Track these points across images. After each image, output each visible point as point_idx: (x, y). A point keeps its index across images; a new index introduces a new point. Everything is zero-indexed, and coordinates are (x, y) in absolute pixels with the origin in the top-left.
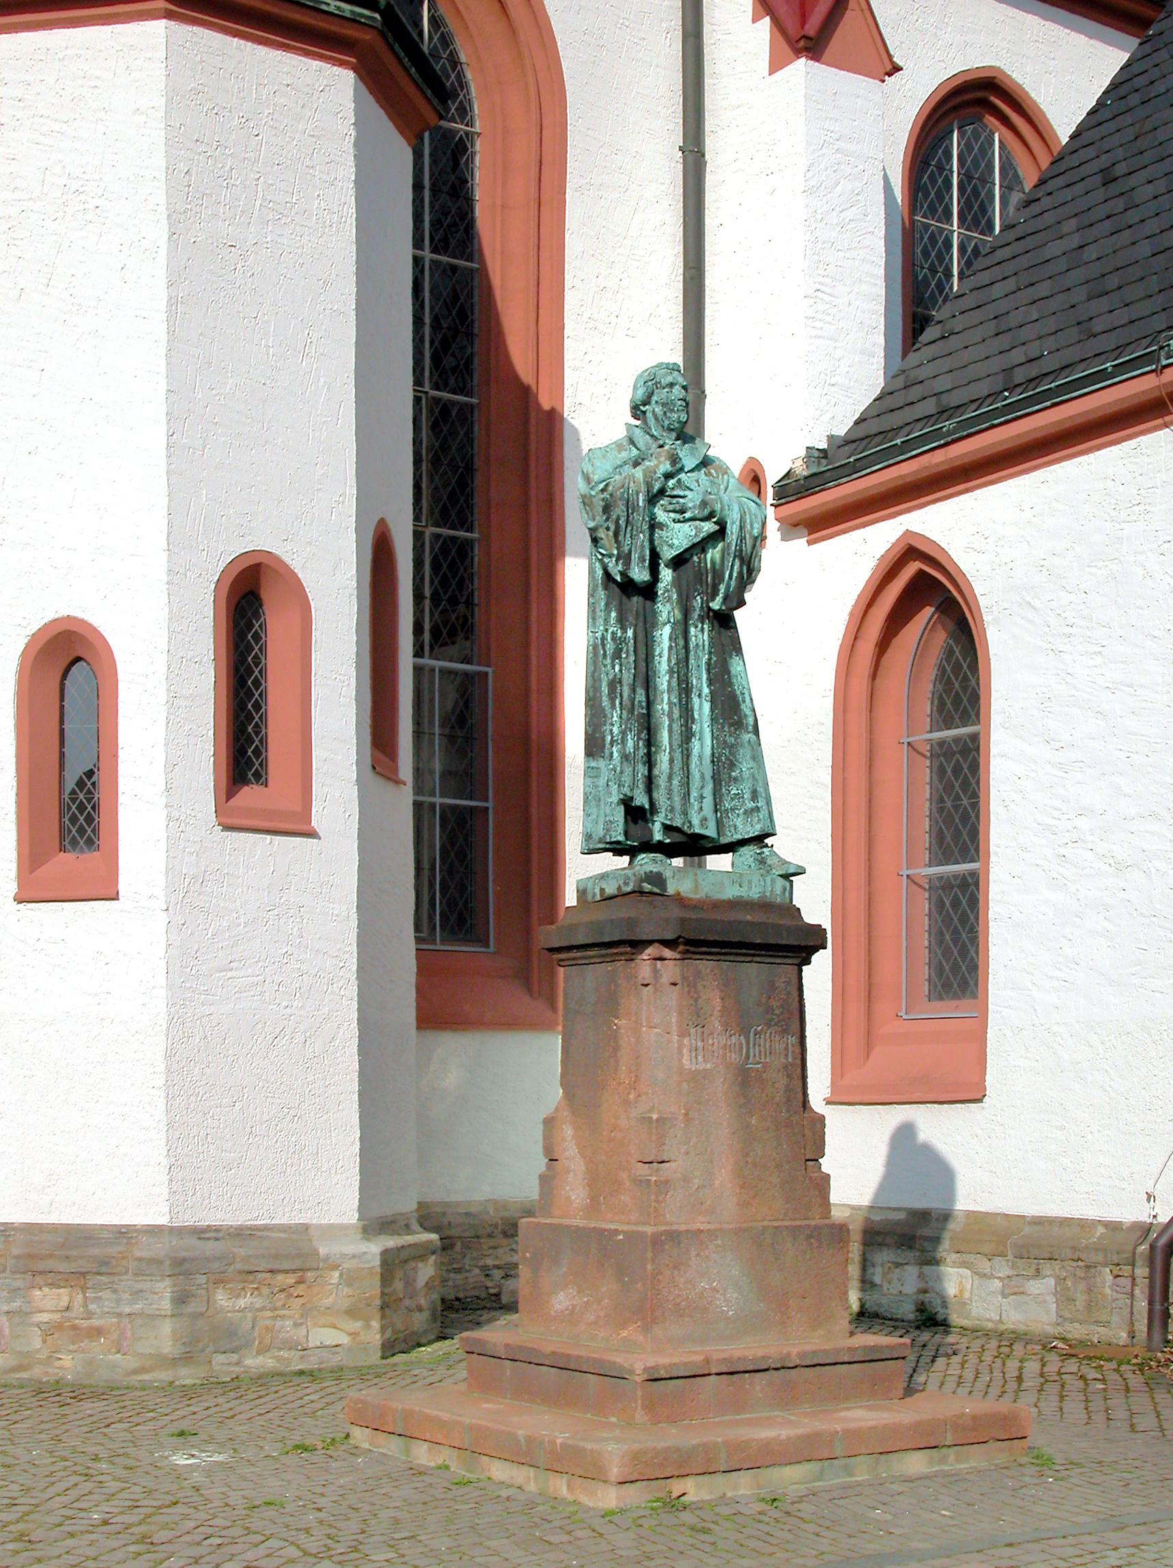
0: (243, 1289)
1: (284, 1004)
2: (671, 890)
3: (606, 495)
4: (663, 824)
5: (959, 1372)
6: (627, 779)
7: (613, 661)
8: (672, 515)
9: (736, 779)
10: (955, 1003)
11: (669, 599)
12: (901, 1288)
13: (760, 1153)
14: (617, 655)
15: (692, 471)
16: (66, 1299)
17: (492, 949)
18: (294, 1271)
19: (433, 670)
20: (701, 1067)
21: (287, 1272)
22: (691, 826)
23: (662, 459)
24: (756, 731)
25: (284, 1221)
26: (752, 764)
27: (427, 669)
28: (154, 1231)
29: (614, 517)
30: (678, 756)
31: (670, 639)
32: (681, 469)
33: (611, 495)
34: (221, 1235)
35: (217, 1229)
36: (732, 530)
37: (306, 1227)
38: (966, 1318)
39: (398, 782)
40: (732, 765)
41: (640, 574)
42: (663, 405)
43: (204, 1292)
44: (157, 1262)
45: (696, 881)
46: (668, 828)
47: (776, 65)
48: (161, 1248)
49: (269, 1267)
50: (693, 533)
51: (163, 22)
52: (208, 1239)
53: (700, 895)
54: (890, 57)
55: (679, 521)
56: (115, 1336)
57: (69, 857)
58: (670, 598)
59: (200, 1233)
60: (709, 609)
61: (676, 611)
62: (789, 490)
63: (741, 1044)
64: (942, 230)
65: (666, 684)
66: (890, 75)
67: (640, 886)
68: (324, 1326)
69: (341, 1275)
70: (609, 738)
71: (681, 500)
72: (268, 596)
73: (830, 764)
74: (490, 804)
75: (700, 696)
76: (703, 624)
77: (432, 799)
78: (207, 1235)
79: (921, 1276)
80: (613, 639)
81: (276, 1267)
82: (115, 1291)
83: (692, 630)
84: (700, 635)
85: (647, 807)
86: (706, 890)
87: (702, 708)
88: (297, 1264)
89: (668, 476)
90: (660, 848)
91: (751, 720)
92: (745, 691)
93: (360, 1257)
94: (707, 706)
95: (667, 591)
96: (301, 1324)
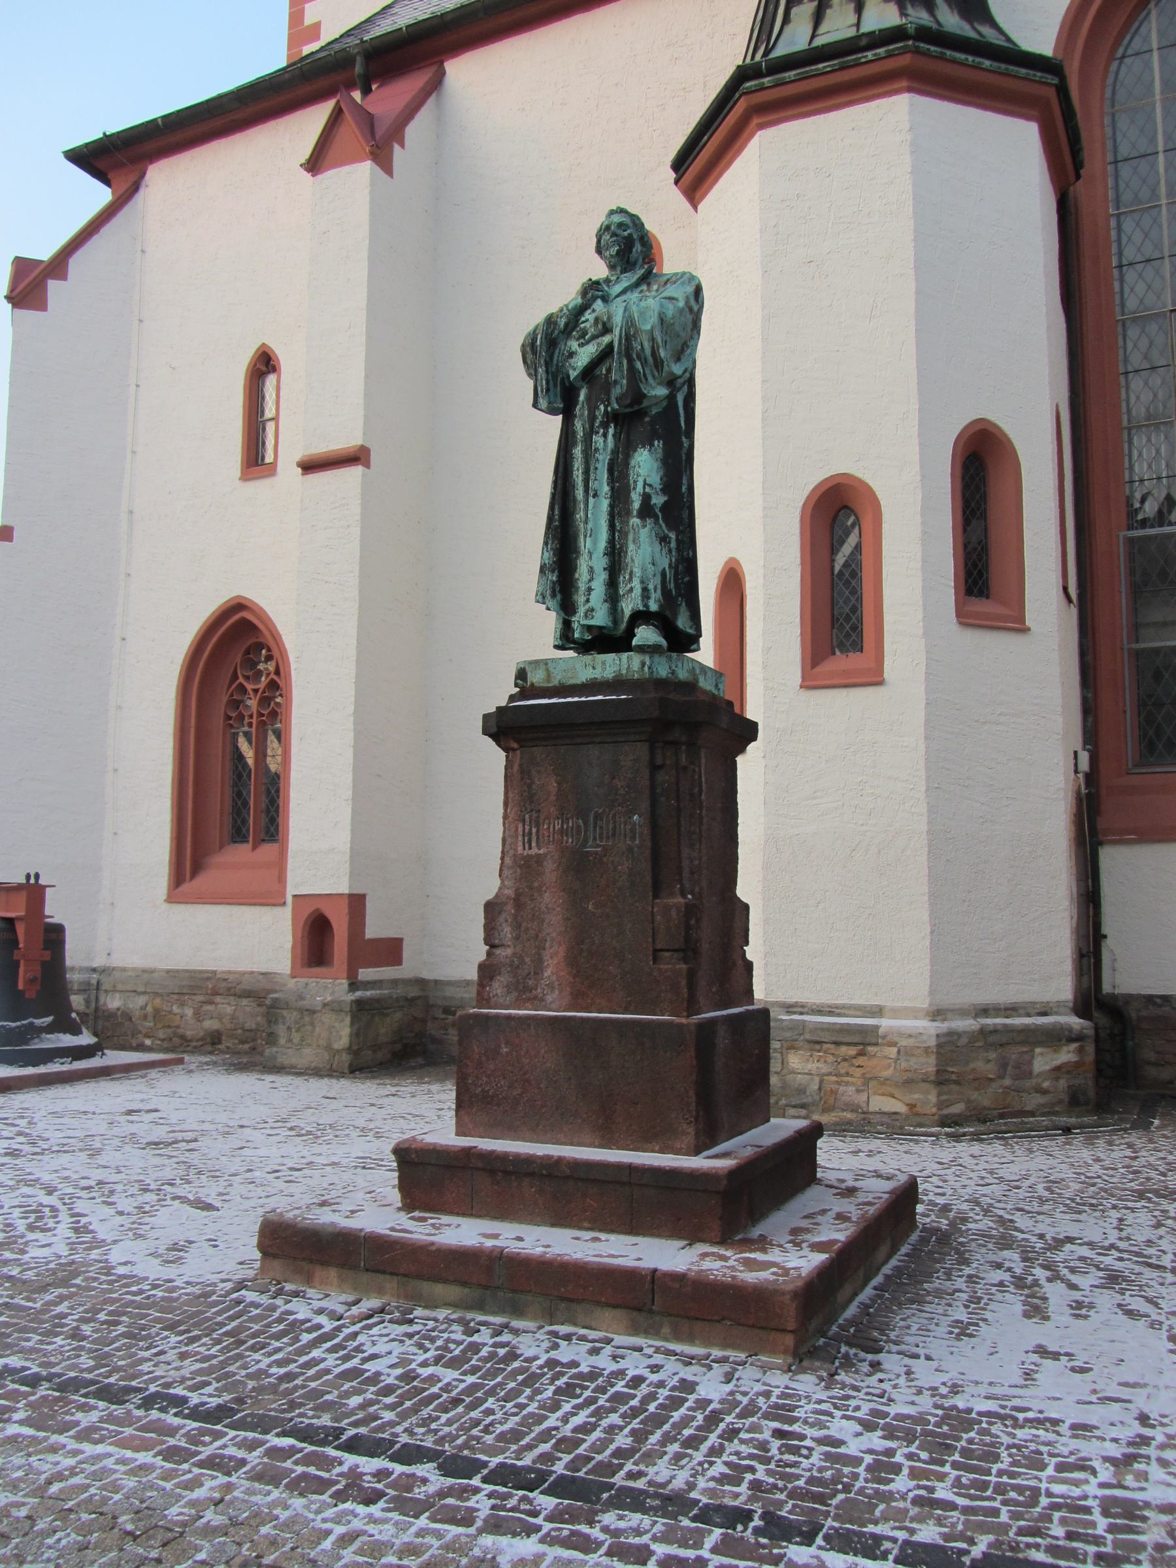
13: (597, 941)
18: (855, 1044)
20: (534, 851)
21: (848, 1044)
34: (805, 1010)
43: (779, 1056)
45: (547, 670)
49: (834, 1039)
63: (579, 827)
68: (883, 1095)
69: (899, 1052)
81: (840, 1039)
86: (559, 677)
88: (857, 1039)
93: (916, 1037)
96: (863, 1091)
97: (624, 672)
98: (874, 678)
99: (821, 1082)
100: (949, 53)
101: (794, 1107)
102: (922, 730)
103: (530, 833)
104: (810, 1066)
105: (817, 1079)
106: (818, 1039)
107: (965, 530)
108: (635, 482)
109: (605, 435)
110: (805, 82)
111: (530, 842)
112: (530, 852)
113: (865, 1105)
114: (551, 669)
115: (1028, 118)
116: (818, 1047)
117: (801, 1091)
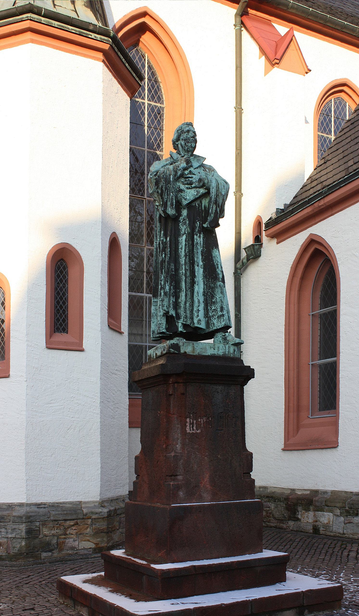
1: (72, 416)
2: (182, 351)
3: (157, 177)
4: (182, 324)
5: (323, 557)
6: (166, 303)
7: (162, 252)
8: (186, 186)
9: (214, 303)
10: (328, 411)
11: (185, 223)
12: (308, 520)
14: (164, 249)
15: (197, 168)
18: (73, 520)
19: (147, 298)
22: (194, 323)
23: (183, 161)
24: (223, 281)
25: (71, 500)
26: (221, 295)
27: (145, 297)
28: (21, 505)
29: (160, 186)
30: (189, 293)
31: (186, 241)
32: (191, 166)
33: (159, 176)
34: (46, 506)
36: (213, 191)
37: (81, 502)
38: (331, 532)
39: (121, 333)
40: (213, 297)
41: (171, 211)
42: (185, 140)
44: (21, 517)
45: (193, 347)
46: (185, 326)
47: (266, 72)
48: (22, 511)
50: (196, 194)
51: (30, 44)
52: (41, 508)
53: (196, 353)
54: (307, 67)
55: (189, 188)
56: (5, 546)
58: (185, 223)
59: (38, 505)
60: (203, 227)
61: (189, 229)
62: (271, 223)
64: (328, 138)
65: (184, 261)
66: (307, 73)
67: (169, 350)
68: (85, 541)
70: (160, 287)
71: (190, 179)
73: (284, 324)
75: (198, 266)
76: (200, 234)
77: (146, 344)
78: (41, 506)
79: (315, 516)
80: (162, 243)
82: (6, 529)
83: (195, 236)
84: (199, 239)
85: (174, 315)
86: (198, 351)
87: (199, 271)
88: (74, 517)
89: (185, 169)
90: (181, 335)
91: (221, 276)
92: (219, 263)
94: (201, 270)
95: (184, 219)
96: (76, 540)
97: (227, 353)
98: (79, 348)
102: (99, 375)
103: (193, 423)
104: (53, 532)
108: (217, 264)
109: (200, 237)
111: (193, 427)
112: (193, 432)
113: (77, 546)
114: (195, 347)
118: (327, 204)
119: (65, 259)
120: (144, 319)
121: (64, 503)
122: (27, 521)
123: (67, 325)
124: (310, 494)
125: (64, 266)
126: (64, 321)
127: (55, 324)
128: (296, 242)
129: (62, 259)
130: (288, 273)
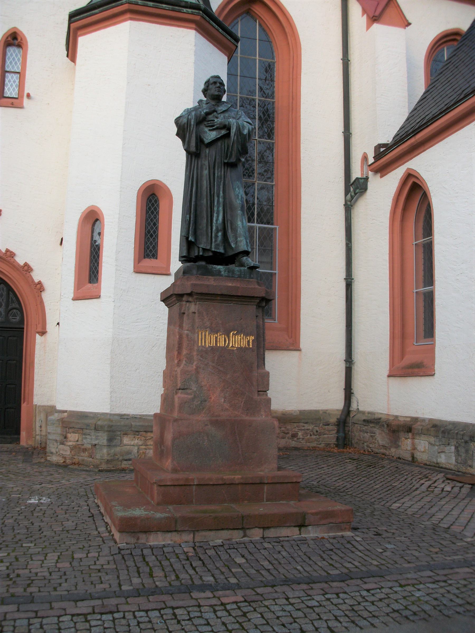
0: (134, 437)
1: (157, 335)
16: (77, 437)
17: (276, 321)
34: (129, 417)
35: (128, 415)
47: (368, 27)
57: (90, 285)
72: (160, 195)
73: (388, 252)
74: (277, 272)
99: (138, 449)
100: (211, 21)
101: (126, 460)
105: (136, 448)
106: (138, 430)
107: (429, 202)
110: (154, 9)
115: (225, 55)
116: (137, 433)
117: (129, 453)
118: (419, 141)
119: (156, 194)
120: (255, 247)
121: (146, 415)
122: (109, 430)
123: (156, 251)
124: (410, 421)
125: (156, 200)
126: (154, 247)
127: (145, 251)
128: (395, 176)
129: (154, 194)
130: (390, 204)
